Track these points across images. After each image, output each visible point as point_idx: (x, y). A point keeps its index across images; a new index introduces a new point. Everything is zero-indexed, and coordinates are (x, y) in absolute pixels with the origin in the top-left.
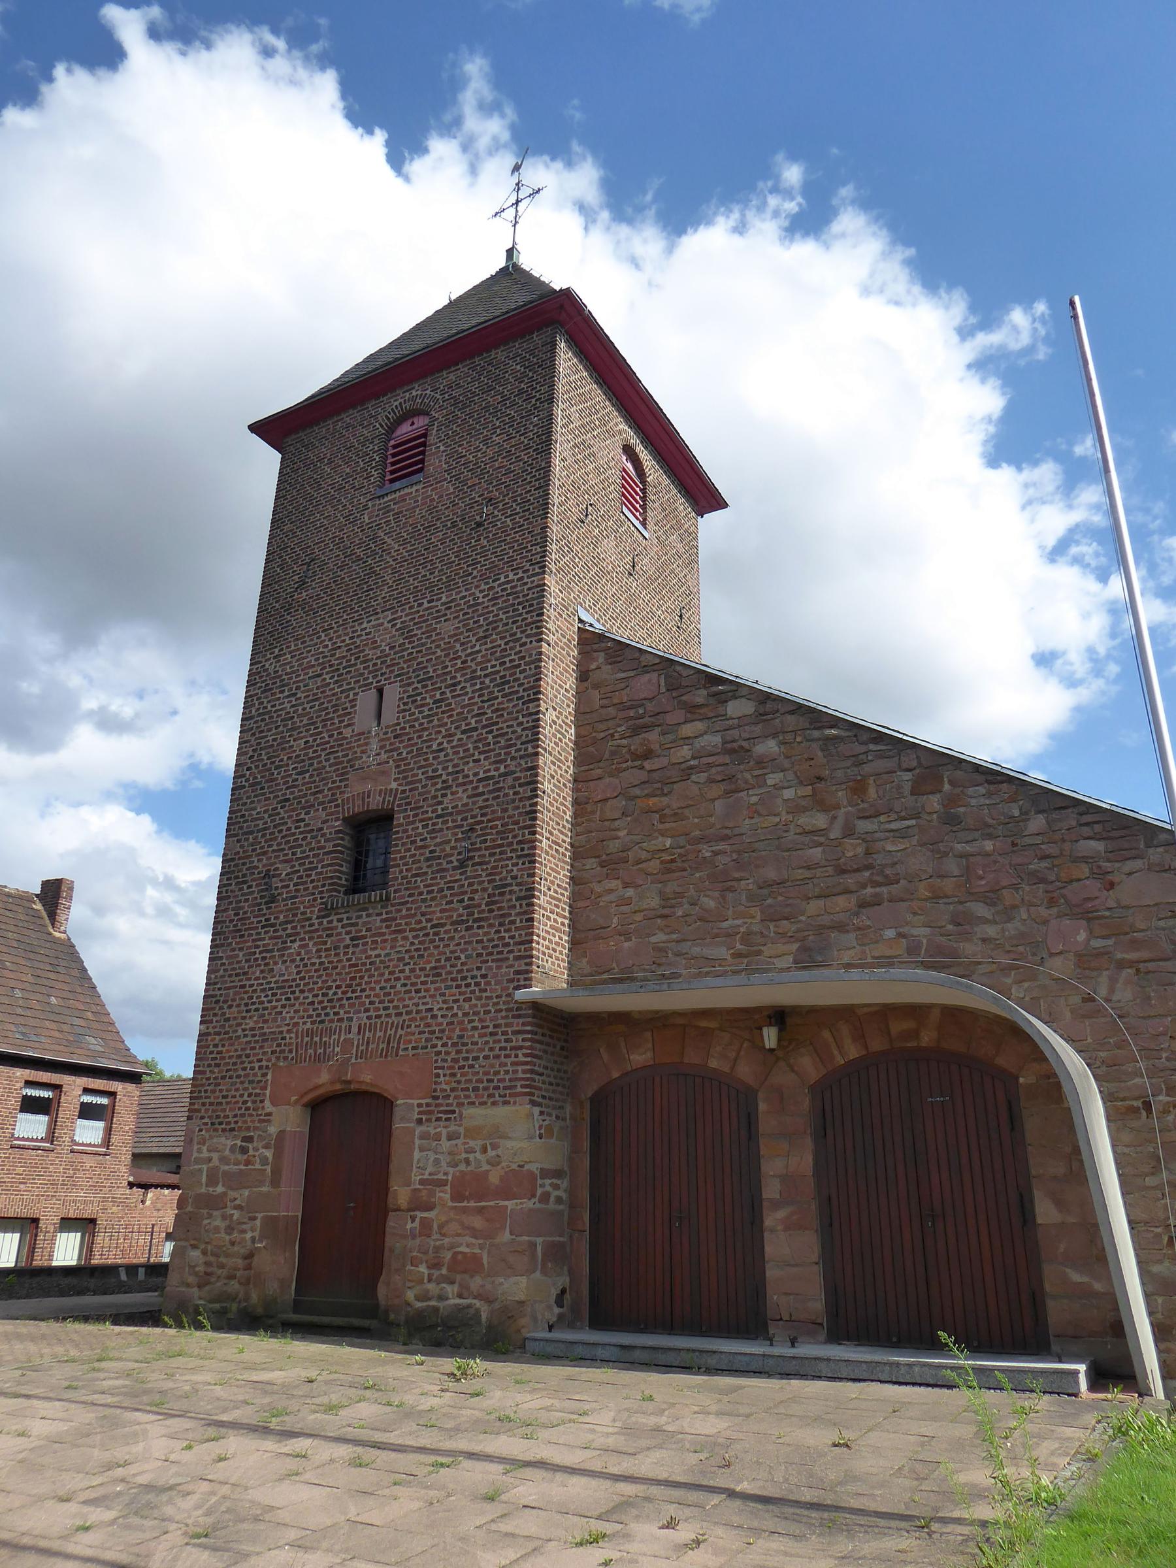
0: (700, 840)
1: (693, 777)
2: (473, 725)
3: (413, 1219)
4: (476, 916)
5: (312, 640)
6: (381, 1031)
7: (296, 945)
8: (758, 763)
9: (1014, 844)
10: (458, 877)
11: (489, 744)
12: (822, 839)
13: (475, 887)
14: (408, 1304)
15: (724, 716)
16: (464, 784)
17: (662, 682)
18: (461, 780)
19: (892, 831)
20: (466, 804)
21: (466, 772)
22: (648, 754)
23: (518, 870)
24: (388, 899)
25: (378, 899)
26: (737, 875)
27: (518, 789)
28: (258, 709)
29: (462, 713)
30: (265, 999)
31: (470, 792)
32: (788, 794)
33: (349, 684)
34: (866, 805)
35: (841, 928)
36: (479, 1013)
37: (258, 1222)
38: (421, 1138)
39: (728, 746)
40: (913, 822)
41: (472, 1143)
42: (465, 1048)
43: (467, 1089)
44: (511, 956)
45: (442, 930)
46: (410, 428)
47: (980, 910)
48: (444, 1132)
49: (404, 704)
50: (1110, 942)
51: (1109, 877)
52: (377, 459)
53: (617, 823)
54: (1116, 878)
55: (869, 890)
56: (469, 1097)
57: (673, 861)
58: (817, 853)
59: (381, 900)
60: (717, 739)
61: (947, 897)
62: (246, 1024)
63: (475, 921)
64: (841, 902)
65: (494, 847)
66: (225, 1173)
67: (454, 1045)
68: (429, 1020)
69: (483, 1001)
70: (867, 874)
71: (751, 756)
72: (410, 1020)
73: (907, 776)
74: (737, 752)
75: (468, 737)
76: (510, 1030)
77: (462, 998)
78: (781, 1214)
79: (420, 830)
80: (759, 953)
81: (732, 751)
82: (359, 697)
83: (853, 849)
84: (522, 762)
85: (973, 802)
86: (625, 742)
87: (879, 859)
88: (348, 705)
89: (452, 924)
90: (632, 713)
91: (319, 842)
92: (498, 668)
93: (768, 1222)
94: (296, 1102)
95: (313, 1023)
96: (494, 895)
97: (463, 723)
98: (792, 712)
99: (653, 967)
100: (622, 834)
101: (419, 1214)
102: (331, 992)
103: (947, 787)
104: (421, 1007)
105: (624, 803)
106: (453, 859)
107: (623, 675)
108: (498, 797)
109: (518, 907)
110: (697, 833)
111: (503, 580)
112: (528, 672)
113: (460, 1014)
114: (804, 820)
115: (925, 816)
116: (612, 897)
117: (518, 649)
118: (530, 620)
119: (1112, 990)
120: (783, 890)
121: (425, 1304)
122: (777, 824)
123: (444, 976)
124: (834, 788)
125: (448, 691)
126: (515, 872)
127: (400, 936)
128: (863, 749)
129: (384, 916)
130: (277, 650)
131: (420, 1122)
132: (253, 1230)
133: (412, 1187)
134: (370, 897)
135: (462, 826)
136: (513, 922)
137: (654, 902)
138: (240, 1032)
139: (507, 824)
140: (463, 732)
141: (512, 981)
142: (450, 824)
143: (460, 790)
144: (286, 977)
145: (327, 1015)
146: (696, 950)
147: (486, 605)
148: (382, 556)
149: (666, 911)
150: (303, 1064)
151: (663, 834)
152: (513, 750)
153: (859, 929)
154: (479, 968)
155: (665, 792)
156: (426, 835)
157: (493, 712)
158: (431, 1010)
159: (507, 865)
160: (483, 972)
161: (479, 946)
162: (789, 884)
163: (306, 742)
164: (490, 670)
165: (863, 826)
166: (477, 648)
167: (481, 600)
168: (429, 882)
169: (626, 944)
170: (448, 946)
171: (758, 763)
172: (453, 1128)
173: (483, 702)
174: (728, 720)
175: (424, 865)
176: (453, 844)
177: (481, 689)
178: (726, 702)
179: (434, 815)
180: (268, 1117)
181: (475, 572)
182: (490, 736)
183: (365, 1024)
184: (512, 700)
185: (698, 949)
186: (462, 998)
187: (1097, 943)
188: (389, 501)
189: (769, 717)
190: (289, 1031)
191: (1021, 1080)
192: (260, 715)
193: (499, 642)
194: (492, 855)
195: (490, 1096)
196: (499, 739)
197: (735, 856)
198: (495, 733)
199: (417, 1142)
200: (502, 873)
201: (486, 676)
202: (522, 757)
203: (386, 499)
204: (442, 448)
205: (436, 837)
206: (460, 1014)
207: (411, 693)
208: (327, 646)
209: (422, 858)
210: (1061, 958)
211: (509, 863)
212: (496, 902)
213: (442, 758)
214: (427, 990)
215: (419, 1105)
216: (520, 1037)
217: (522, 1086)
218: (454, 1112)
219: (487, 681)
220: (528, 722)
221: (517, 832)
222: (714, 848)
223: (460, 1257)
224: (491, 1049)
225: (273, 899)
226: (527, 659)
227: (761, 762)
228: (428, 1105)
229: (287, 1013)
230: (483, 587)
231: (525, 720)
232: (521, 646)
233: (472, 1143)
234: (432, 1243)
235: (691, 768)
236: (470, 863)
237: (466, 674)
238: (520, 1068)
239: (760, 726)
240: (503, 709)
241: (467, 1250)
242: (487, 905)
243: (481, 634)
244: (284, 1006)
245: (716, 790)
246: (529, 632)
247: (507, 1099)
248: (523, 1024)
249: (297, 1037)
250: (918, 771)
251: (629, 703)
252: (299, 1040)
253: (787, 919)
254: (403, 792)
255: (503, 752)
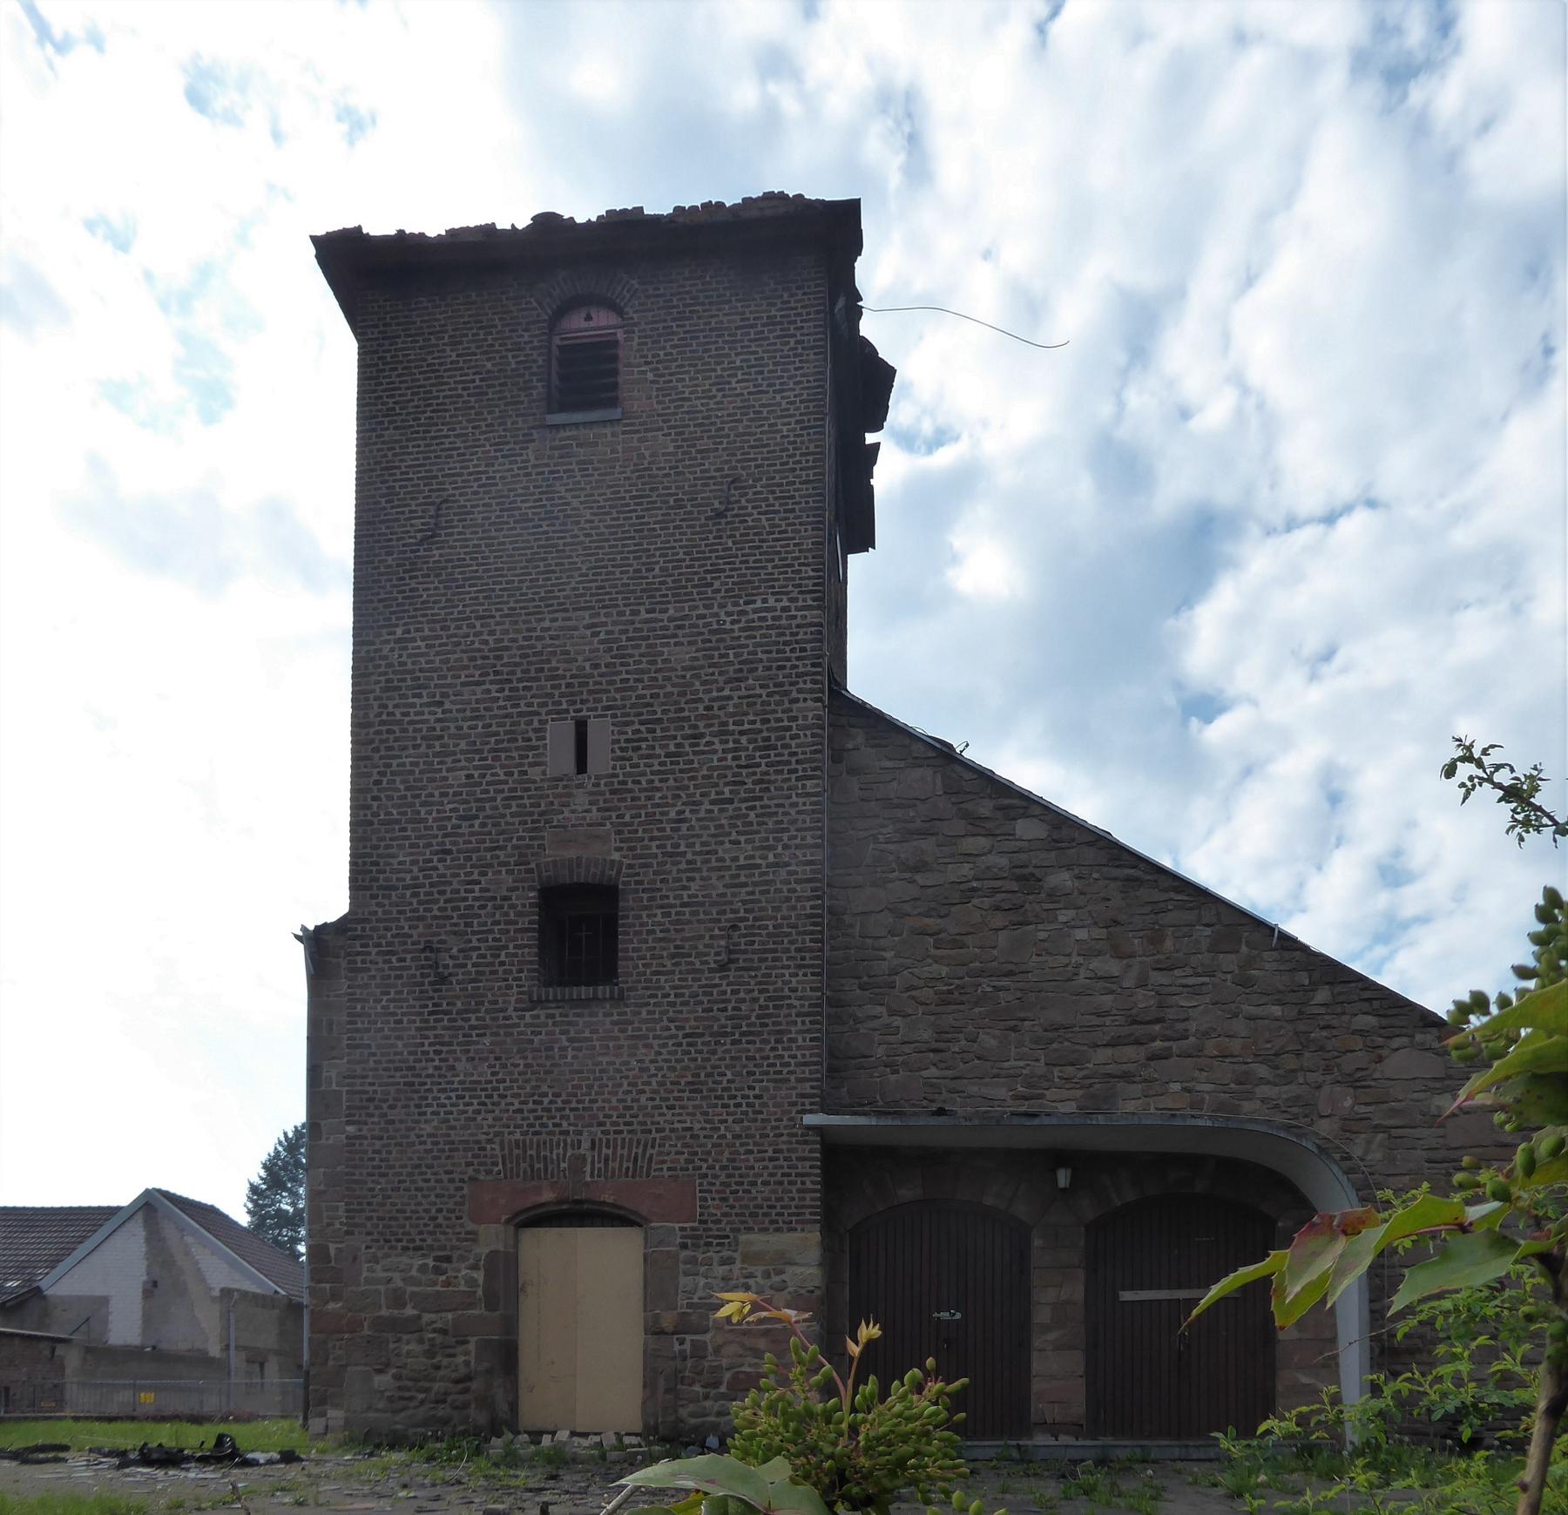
0: (981, 973)
1: (975, 901)
2: (727, 795)
3: (682, 1342)
4: (744, 1029)
5: (459, 627)
6: (623, 1148)
7: (487, 1041)
8: (1049, 895)
9: (1300, 1012)
10: (717, 981)
11: (751, 824)
12: (1114, 987)
13: (742, 995)
14: (682, 1421)
15: (1011, 835)
16: (720, 869)
17: (939, 781)
18: (714, 864)
19: (1187, 986)
20: (723, 895)
21: (720, 854)
22: (921, 867)
23: (798, 982)
24: (621, 998)
25: (608, 996)
26: (1022, 1015)
27: (793, 885)
28: (380, 714)
29: (710, 777)
30: (447, 1102)
31: (727, 880)
32: (1081, 934)
33: (529, 705)
34: (1161, 957)
35: (1126, 1077)
36: (754, 1136)
37: (471, 1347)
38: (685, 1263)
39: (1017, 871)
40: (1206, 979)
41: (751, 1269)
42: (737, 1172)
43: (742, 1215)
44: (793, 1078)
45: (699, 1041)
46: (584, 325)
47: (1262, 1071)
48: (716, 1257)
49: (622, 750)
50: (1370, 1109)
51: (1379, 1051)
52: (541, 363)
53: (882, 942)
54: (1384, 1052)
55: (1158, 1044)
56: (746, 1222)
57: (950, 992)
58: (1107, 1001)
59: (612, 998)
60: (1004, 861)
61: (1233, 1056)
62: (421, 1129)
63: (743, 1034)
64: (1130, 1051)
65: (765, 951)
66: (413, 1294)
67: (723, 1168)
68: (688, 1140)
69: (759, 1124)
70: (1157, 1027)
71: (1042, 887)
72: (662, 1138)
73: (1208, 931)
74: (1028, 880)
75: (721, 810)
76: (794, 1156)
77: (730, 1119)
78: (1051, 1336)
79: (659, 918)
80: (1042, 1096)
81: (1018, 878)
82: (548, 727)
83: (1144, 1000)
84: (798, 853)
85: (1267, 966)
86: (891, 847)
87: (1171, 1014)
88: (531, 735)
89: (711, 1035)
90: (899, 813)
91: (507, 914)
92: (758, 725)
93: (1037, 1342)
94: (508, 1221)
95: (525, 1133)
96: (767, 1007)
97: (713, 790)
98: (1089, 844)
99: (925, 1103)
100: (889, 955)
101: (688, 1338)
102: (546, 1100)
103: (1244, 949)
104: (677, 1125)
105: (891, 920)
106: (710, 959)
107: (889, 764)
108: (768, 892)
109: (799, 1024)
110: (977, 964)
111: (759, 604)
112: (802, 739)
113: (729, 1136)
114: (1095, 964)
115: (1220, 975)
116: (875, 1024)
117: (787, 705)
118: (801, 670)
119: (1367, 1152)
120: (1070, 1035)
121: (700, 1420)
122: (1067, 966)
123: (705, 1093)
124: (1131, 934)
125: (686, 743)
126: (794, 985)
127: (640, 1044)
128: (1165, 896)
129: (615, 1018)
130: (399, 631)
131: (684, 1246)
132: (467, 1353)
133: (679, 1310)
134: (595, 992)
135: (719, 921)
136: (792, 1040)
137: (927, 1035)
138: (413, 1138)
139: (781, 926)
140: (712, 803)
141: (794, 1104)
142: (702, 916)
143: (714, 875)
144: (475, 1078)
145: (543, 1125)
146: (974, 1089)
147: (736, 634)
148: (564, 524)
149: (942, 1045)
150: (623, 1178)
151: (937, 960)
152: (785, 836)
153: (1146, 1081)
154: (751, 1088)
155: (942, 913)
156: (667, 925)
157: (754, 783)
158: (690, 1129)
159: (783, 975)
160: (757, 1092)
161: (751, 1064)
162: (1077, 1029)
163: (468, 777)
164: (746, 726)
165: (1157, 978)
166: (726, 693)
167: (728, 626)
168: (677, 982)
169: (893, 1077)
170: (708, 1060)
171: (1049, 895)
172: (726, 1253)
173: (739, 767)
174: (1017, 840)
175: (668, 963)
176: (707, 940)
177: (735, 750)
178: (1015, 819)
179: (678, 902)
180: (473, 1237)
181: (717, 584)
182: (752, 814)
183: (600, 1140)
184: (781, 772)
185: (976, 1089)
186: (730, 1119)
187: (1363, 1109)
188: (568, 438)
189: (1063, 845)
190: (489, 1141)
191: (1280, 1224)
192: (383, 723)
193: (758, 691)
194: (762, 960)
195: (772, 1222)
196: (765, 819)
197: (1019, 994)
198: (759, 811)
199: (682, 1266)
200: (775, 983)
201: (742, 733)
202: (797, 847)
203: (563, 434)
204: (650, 376)
205: (683, 930)
206: (729, 1136)
207: (630, 735)
208: (486, 642)
209: (665, 954)
210: (1328, 1120)
211: (786, 972)
212: (769, 1016)
213: (684, 831)
214: (682, 1107)
215: (682, 1229)
216: (808, 1164)
217: (811, 1214)
218: (728, 1237)
219: (744, 740)
220: (804, 804)
221: (795, 937)
222: (996, 983)
223: (741, 1376)
224: (771, 1175)
225: (443, 980)
226: (800, 722)
227: (1053, 895)
228: (693, 1229)
229: (484, 1119)
230: (730, 608)
231: (801, 800)
232: (791, 702)
233: (751, 1269)
234: (706, 1364)
235: (974, 889)
236: (733, 966)
237: (712, 725)
238: (808, 1196)
239: (1053, 854)
240: (769, 782)
241: (749, 1370)
242: (758, 1017)
243: (732, 674)
244: (478, 1112)
245: (999, 920)
246: (801, 685)
247: (794, 1225)
248: (811, 1151)
249: (502, 1149)
250: (1217, 927)
251: (895, 801)
252: (506, 1152)
253: (1072, 1064)
254: (630, 866)
255: (771, 836)
